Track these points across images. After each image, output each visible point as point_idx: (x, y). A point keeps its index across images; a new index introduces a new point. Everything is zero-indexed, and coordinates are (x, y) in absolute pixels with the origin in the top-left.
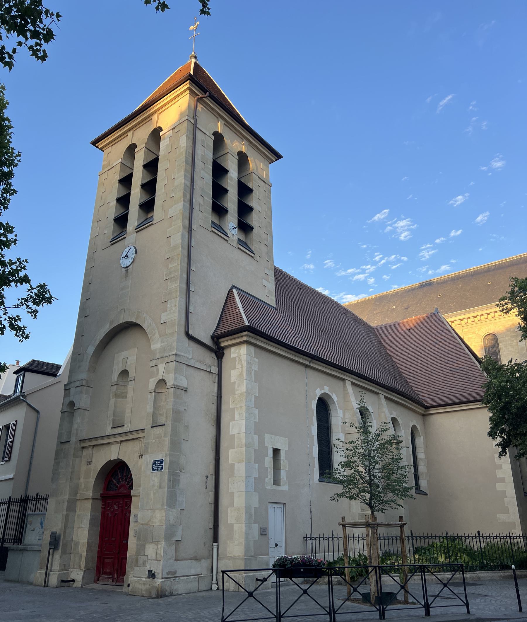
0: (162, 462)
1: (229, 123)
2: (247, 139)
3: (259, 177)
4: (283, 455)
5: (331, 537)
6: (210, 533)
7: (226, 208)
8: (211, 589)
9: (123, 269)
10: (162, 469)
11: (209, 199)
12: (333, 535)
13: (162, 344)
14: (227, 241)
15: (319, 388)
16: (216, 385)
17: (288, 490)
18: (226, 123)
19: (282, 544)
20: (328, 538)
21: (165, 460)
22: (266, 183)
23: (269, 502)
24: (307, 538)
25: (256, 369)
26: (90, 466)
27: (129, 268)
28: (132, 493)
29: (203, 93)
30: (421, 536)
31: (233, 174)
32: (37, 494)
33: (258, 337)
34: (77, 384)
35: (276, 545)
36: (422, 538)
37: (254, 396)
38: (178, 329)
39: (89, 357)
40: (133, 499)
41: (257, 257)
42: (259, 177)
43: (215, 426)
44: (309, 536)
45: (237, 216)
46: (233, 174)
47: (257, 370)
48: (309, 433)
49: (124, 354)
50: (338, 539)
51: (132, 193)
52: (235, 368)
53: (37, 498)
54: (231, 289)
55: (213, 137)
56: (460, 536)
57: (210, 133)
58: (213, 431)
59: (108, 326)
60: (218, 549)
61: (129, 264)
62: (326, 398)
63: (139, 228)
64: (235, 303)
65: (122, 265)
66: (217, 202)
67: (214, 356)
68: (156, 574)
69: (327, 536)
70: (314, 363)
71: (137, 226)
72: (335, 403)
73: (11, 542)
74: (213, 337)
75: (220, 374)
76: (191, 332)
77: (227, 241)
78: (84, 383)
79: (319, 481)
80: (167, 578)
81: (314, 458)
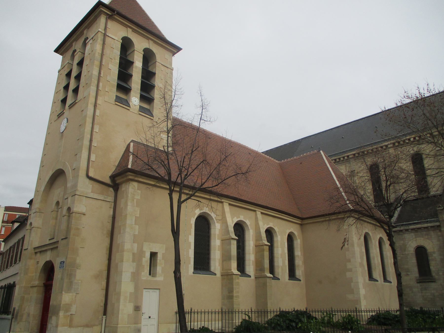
3: (162, 64)
4: (159, 256)
5: (279, 311)
6: (102, 309)
12: (251, 310)
14: (129, 110)
16: (112, 210)
17: (163, 280)
18: (133, 31)
20: (188, 312)
21: (66, 261)
25: (139, 197)
27: (64, 133)
29: (113, 13)
30: (310, 310)
35: (150, 317)
36: (365, 311)
38: (84, 173)
42: (162, 64)
47: (140, 198)
50: (205, 313)
55: (122, 41)
56: (368, 310)
58: (108, 241)
60: (106, 320)
62: (241, 223)
64: (134, 151)
67: (111, 189)
69: (248, 311)
75: (115, 202)
77: (129, 110)
81: (190, 258)
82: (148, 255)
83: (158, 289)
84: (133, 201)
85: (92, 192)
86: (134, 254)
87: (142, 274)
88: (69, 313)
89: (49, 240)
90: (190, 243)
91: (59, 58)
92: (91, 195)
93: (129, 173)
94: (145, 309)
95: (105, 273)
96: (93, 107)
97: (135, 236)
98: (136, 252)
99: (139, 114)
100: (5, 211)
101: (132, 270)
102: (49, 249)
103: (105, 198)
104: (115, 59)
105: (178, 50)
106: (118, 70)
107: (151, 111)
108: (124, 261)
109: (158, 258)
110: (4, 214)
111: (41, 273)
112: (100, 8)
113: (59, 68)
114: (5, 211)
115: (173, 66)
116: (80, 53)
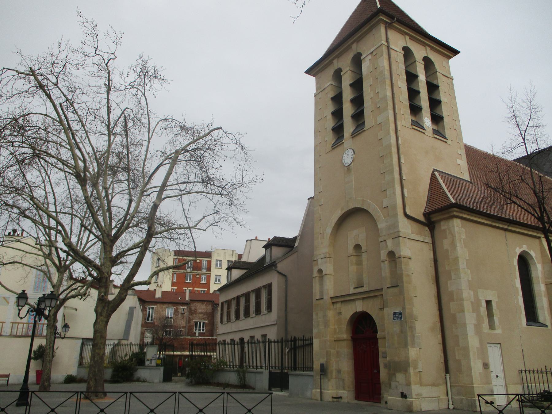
0: (400, 313)
1: (413, 37)
2: (429, 46)
3: (442, 74)
4: (494, 304)
6: (442, 366)
7: (419, 106)
8: (449, 408)
9: (345, 167)
10: (401, 318)
11: (407, 103)
12: (546, 370)
13: (387, 224)
14: (424, 133)
15: (518, 247)
19: (501, 375)
22: (448, 77)
23: (488, 343)
24: (522, 371)
26: (340, 316)
27: (351, 165)
28: (379, 335)
30: (538, 370)
31: (422, 77)
32: (304, 336)
33: (464, 211)
34: (322, 256)
35: (497, 376)
37: (466, 259)
39: (329, 236)
40: (379, 341)
41: (449, 142)
42: (442, 74)
43: (435, 284)
44: (523, 369)
45: (429, 111)
46: (422, 77)
47: (465, 238)
48: (514, 286)
49: (355, 232)
51: (344, 107)
52: (446, 238)
53: (304, 339)
54: (433, 172)
57: (399, 49)
59: (340, 212)
60: (450, 378)
61: (350, 163)
63: (354, 135)
65: (344, 164)
66: (413, 104)
67: (427, 228)
68: (407, 395)
70: (512, 226)
71: (352, 132)
72: (533, 258)
73: (280, 369)
74: (425, 215)
76: (408, 213)
78: (328, 256)
79: (527, 325)
80: (416, 398)
81: (520, 306)
82: (484, 304)
83: (498, 344)
84: (461, 241)
85: (412, 233)
86: (472, 303)
87: (483, 326)
88: (417, 370)
89: (354, 288)
90: (517, 288)
91: (312, 80)
92: (413, 236)
93: (455, 209)
94: (492, 367)
95: (439, 325)
96: (395, 134)
97: (469, 281)
98: (473, 301)
99: (434, 137)
100: (174, 256)
101: (474, 322)
102: (359, 299)
103: (424, 239)
104: (402, 75)
105: (455, 54)
106: (407, 87)
107: (442, 133)
108: (465, 311)
109: (494, 308)
110: (174, 259)
111: (347, 326)
112: (379, 16)
113: (314, 91)
114: (174, 256)
115: (452, 74)
116: (350, 72)
